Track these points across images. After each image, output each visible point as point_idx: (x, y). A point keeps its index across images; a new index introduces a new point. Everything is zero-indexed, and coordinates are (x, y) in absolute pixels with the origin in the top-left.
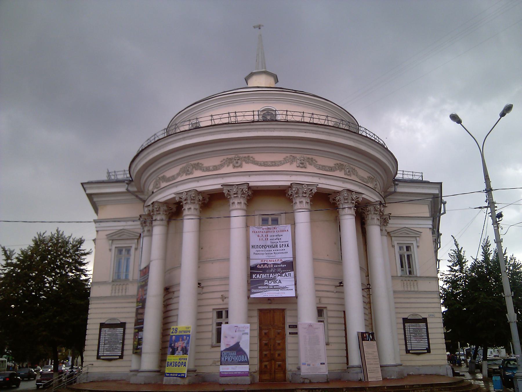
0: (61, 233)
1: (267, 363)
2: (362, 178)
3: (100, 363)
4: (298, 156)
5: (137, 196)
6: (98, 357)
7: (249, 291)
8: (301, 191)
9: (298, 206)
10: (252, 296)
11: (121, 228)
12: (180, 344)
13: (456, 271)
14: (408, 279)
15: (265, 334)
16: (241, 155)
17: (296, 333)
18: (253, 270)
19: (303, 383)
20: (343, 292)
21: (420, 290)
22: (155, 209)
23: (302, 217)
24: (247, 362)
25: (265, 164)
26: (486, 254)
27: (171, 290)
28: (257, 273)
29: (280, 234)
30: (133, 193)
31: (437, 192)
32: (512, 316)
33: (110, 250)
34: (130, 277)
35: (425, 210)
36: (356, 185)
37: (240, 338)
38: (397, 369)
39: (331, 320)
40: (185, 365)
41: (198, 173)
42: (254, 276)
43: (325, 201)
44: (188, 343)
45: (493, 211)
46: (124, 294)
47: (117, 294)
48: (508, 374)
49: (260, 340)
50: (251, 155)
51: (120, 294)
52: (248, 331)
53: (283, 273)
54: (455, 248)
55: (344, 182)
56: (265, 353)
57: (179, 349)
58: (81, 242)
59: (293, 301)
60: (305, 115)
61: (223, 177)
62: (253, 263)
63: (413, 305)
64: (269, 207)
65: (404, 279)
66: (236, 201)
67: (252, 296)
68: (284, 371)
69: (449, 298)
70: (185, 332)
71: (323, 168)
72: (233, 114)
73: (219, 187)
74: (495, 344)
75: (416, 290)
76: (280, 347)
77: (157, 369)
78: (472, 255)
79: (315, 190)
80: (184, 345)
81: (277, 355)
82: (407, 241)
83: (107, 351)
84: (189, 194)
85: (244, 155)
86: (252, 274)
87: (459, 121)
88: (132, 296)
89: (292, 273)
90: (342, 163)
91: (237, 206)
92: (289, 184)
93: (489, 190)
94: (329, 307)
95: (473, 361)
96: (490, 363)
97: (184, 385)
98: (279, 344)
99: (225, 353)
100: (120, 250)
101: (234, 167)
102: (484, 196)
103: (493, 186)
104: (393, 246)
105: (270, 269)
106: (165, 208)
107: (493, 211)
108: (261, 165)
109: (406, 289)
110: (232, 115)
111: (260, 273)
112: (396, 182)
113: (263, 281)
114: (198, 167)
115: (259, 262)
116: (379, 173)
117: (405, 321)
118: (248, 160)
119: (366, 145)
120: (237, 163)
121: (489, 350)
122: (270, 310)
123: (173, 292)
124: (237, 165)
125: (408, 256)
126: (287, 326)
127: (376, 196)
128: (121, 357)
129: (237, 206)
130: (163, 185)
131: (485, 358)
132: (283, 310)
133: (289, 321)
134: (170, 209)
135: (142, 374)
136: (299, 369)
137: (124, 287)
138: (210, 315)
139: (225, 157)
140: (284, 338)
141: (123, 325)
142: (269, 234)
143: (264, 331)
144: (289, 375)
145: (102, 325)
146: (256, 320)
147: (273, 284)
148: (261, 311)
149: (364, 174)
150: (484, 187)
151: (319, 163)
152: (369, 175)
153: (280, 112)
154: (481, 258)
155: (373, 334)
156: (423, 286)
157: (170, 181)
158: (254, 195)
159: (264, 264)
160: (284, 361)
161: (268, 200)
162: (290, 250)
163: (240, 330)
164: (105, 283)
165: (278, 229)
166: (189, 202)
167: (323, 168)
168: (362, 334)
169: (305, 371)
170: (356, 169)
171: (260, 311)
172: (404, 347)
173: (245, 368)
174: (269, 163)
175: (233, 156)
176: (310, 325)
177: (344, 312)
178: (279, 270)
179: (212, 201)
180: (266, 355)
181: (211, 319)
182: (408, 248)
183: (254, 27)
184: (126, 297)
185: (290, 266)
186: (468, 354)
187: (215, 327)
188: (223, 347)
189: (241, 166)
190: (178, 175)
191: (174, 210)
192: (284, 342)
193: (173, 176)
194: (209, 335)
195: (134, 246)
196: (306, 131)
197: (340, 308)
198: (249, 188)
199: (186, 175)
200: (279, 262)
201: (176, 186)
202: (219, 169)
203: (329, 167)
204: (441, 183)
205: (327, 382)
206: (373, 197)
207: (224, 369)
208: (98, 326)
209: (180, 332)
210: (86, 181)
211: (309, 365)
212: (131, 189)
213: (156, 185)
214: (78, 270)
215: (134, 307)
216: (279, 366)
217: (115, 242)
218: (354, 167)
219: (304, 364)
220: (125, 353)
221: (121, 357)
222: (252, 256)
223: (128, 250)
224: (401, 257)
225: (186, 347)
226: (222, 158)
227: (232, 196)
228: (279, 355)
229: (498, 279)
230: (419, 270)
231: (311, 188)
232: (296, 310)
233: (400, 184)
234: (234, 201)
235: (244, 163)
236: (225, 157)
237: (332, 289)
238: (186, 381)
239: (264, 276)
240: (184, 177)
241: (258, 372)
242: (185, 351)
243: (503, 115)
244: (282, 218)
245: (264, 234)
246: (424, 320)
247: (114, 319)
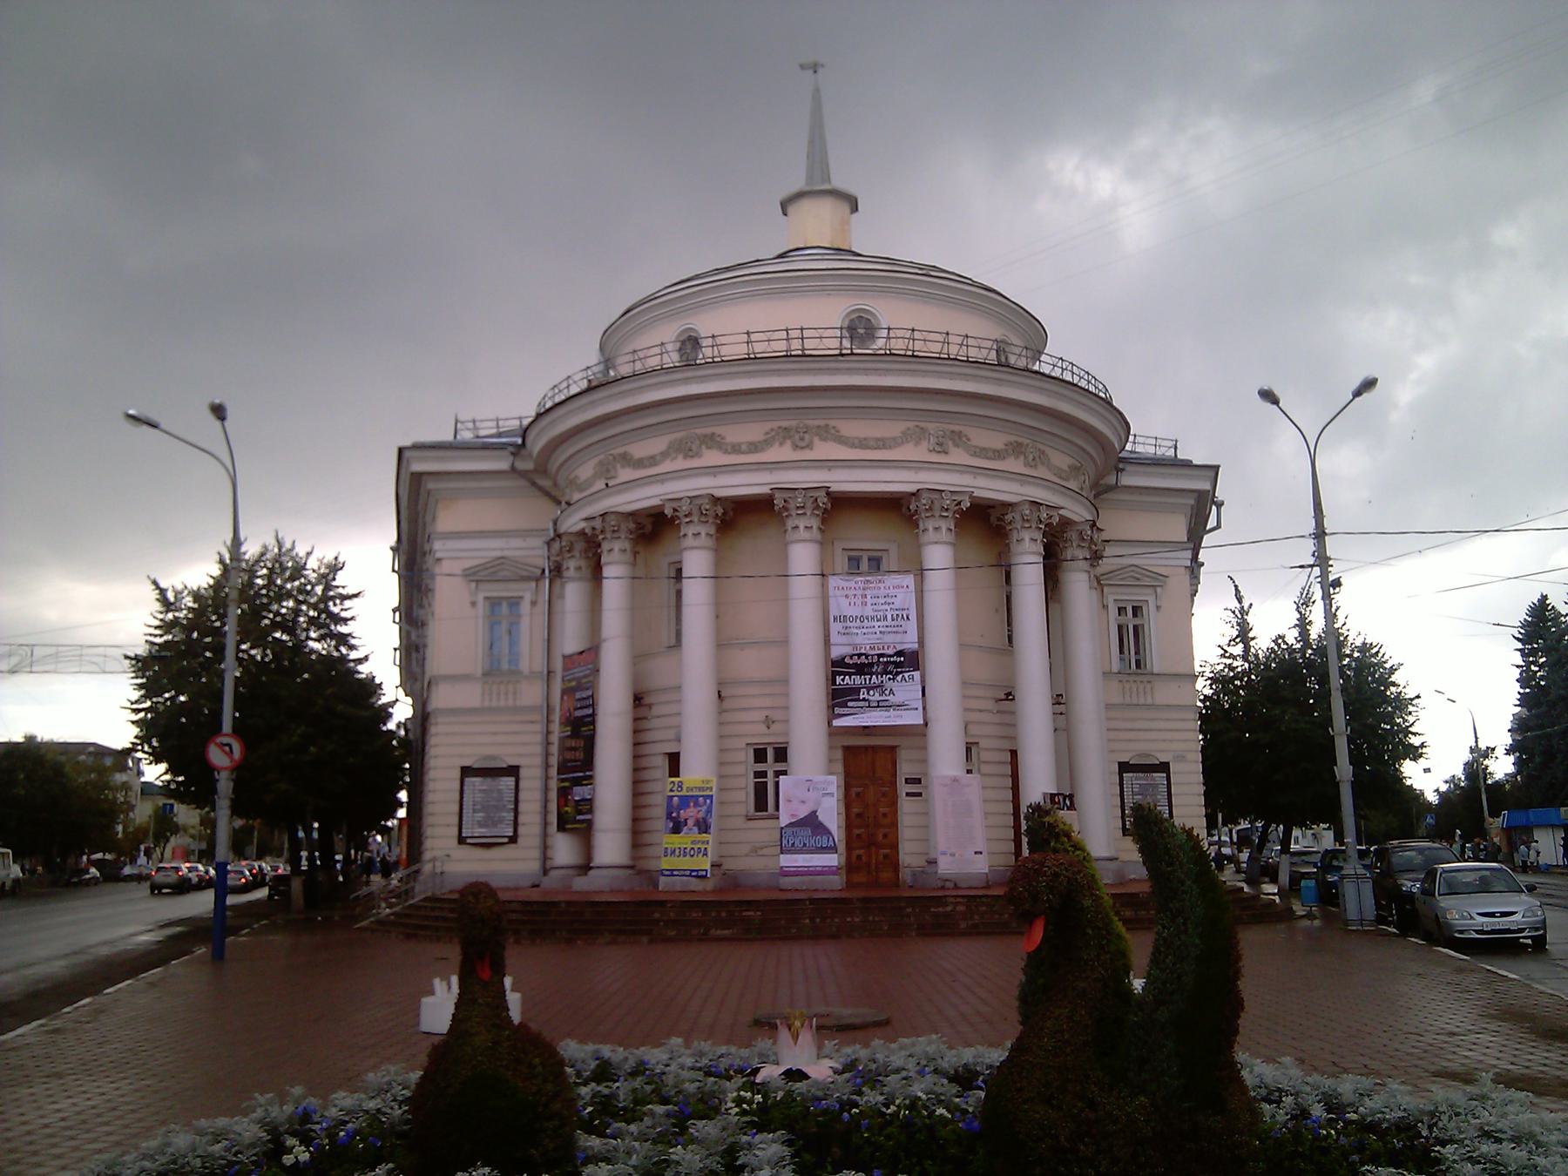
0: (288, 545)
1: (861, 852)
2: (1058, 472)
3: (465, 852)
4: (931, 427)
5: (534, 484)
6: (462, 840)
7: (833, 715)
8: (937, 506)
9: (931, 535)
10: (836, 723)
11: (499, 554)
12: (690, 813)
13: (1234, 658)
14: (1132, 678)
15: (858, 794)
16: (810, 423)
17: (920, 794)
18: (838, 666)
19: (943, 888)
20: (1013, 713)
21: (1158, 702)
22: (609, 529)
23: (938, 554)
24: (833, 849)
25: (863, 444)
26: (1303, 625)
27: (647, 700)
28: (845, 674)
29: (892, 592)
30: (523, 474)
31: (1207, 486)
32: (1344, 769)
33: (473, 604)
34: (524, 666)
35: (1177, 529)
36: (1048, 488)
37: (819, 803)
38: (1112, 865)
39: (985, 769)
40: (705, 854)
41: (712, 457)
42: (839, 679)
43: (984, 523)
44: (709, 811)
45: (1324, 574)
46: (510, 702)
47: (494, 704)
48: (1330, 878)
49: (848, 807)
50: (832, 423)
51: (502, 703)
52: (833, 789)
53: (898, 674)
54: (1235, 604)
55: (1022, 483)
56: (857, 831)
57: (690, 822)
58: (335, 568)
59: (919, 733)
60: (952, 339)
61: (771, 470)
62: (836, 652)
63: (1142, 735)
64: (865, 535)
65: (1125, 678)
66: (802, 523)
67: (836, 723)
68: (896, 866)
69: (1214, 718)
70: (700, 789)
71: (982, 452)
72: (797, 333)
73: (765, 490)
74: (1304, 819)
75: (1149, 701)
76: (887, 821)
77: (629, 863)
78: (1273, 624)
79: (966, 504)
80: (701, 815)
81: (880, 837)
82: (1132, 596)
83: (481, 825)
84: (699, 502)
85: (817, 423)
86: (834, 674)
87: (1275, 402)
88: (531, 709)
89: (917, 674)
90: (1020, 440)
91: (802, 533)
92: (911, 488)
93: (1320, 535)
94: (984, 743)
95: (1256, 855)
96: (1295, 859)
97: (705, 892)
98: (885, 815)
99: (789, 831)
100: (494, 603)
101: (796, 447)
102: (1310, 545)
103: (1328, 525)
104: (1105, 607)
105: (872, 665)
106: (632, 526)
107: (1324, 574)
108: (853, 446)
109: (1128, 700)
110: (793, 334)
111: (850, 674)
112: (1122, 463)
113: (856, 690)
114: (712, 441)
115: (848, 650)
116: (1091, 457)
117: (1124, 767)
118: (827, 434)
119: (1071, 400)
120: (802, 439)
121: (1296, 832)
122: (866, 748)
123: (650, 706)
124: (802, 444)
125: (1136, 628)
126: (901, 781)
127: (1077, 496)
128: (513, 839)
129: (802, 533)
130: (625, 474)
131: (1285, 848)
132: (893, 749)
133: (905, 769)
134: (640, 526)
135: (605, 872)
136: (933, 862)
137: (511, 687)
138: (741, 756)
139: (775, 425)
140: (894, 803)
141: (513, 771)
142: (868, 592)
143: (854, 791)
144: (905, 875)
145: (466, 771)
146: (840, 768)
147: (877, 697)
148: (848, 750)
149: (1061, 460)
150: (1310, 526)
151: (974, 443)
152: (1070, 461)
153: (900, 333)
154: (1292, 637)
155: (1071, 797)
156: (1165, 694)
157: (645, 467)
158: (839, 507)
159: (859, 655)
160: (895, 847)
161: (873, 520)
162: (912, 626)
163: (812, 786)
164: (466, 678)
165: (888, 584)
166: (695, 519)
167: (982, 452)
168: (1053, 796)
169: (946, 867)
170: (1049, 451)
171: (848, 750)
172: (455, 831)
173: (832, 860)
174: (872, 443)
175: (794, 423)
176: (955, 780)
177: (1014, 753)
178: (890, 668)
179: (739, 516)
180: (859, 836)
181: (745, 767)
182: (1136, 611)
183: (802, 67)
184: (516, 710)
185: (910, 661)
186: (1243, 840)
187: (751, 780)
188: (784, 820)
189: (809, 446)
190: (665, 455)
191: (591, 545)
192: (896, 812)
193: (652, 457)
194: (741, 796)
195: (528, 597)
196: (951, 376)
197: (1008, 745)
198: (828, 494)
199: (685, 457)
200: (891, 652)
201: (662, 482)
202: (762, 450)
203: (994, 451)
204: (1215, 469)
205: (987, 887)
206: (1077, 511)
207: (787, 861)
208: (457, 774)
209: (689, 789)
210: (408, 443)
211: (953, 855)
212: (520, 465)
213: (606, 470)
214: (332, 635)
215: (535, 733)
216: (886, 856)
217: (482, 586)
218: (1042, 447)
219: (944, 853)
220: (521, 830)
221: (513, 839)
222: (834, 638)
223: (514, 602)
224: (1120, 627)
225: (704, 820)
226: (768, 426)
227: (794, 513)
228: (885, 836)
229: (1324, 680)
230: (1157, 660)
231: (958, 498)
232: (924, 748)
233: (1129, 468)
234: (796, 522)
235: (816, 440)
236: (775, 425)
237: (991, 705)
238: (709, 885)
239: (858, 680)
240: (680, 463)
241: (843, 872)
242: (703, 826)
243: (1358, 393)
244: (890, 561)
245: (859, 592)
246: (1164, 767)
247: (493, 758)
